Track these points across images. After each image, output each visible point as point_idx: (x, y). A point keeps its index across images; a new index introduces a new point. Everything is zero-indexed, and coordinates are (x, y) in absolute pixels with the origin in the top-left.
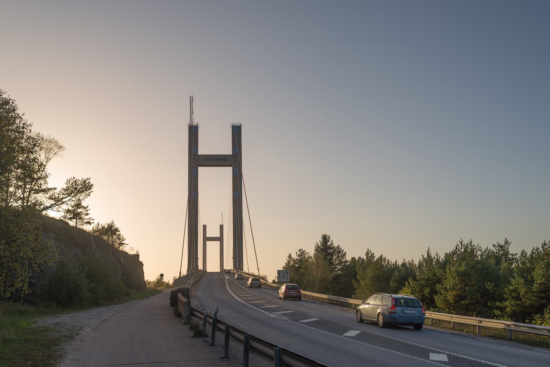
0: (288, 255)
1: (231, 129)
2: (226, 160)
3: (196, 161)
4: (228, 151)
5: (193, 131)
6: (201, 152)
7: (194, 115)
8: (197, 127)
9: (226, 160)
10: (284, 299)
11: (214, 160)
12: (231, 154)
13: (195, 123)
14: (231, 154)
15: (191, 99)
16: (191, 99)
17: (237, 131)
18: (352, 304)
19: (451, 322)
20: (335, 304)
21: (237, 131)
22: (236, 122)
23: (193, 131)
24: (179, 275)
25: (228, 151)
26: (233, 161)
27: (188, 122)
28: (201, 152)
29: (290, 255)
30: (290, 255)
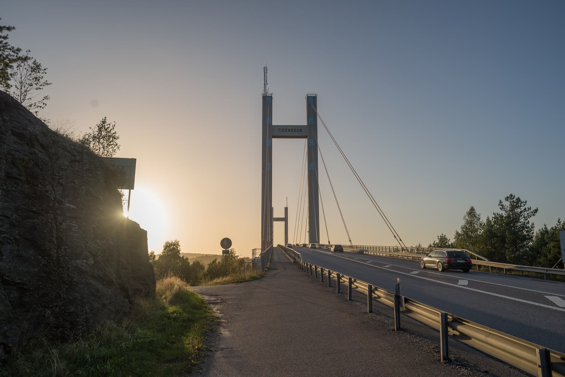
0: (468, 210)
1: (306, 100)
2: (301, 130)
3: (271, 132)
4: (303, 122)
5: (267, 101)
6: (276, 122)
7: (268, 86)
8: (271, 98)
9: (301, 130)
10: (444, 270)
11: (289, 130)
12: (306, 124)
13: (270, 92)
14: (306, 124)
15: (265, 70)
16: (265, 70)
17: (312, 102)
18: (475, 265)
19: (503, 269)
20: (559, 280)
21: (312, 102)
22: (312, 92)
23: (267, 101)
24: (257, 244)
25: (303, 122)
26: (308, 132)
27: (262, 91)
28: (276, 122)
29: (472, 209)
30: (472, 209)
